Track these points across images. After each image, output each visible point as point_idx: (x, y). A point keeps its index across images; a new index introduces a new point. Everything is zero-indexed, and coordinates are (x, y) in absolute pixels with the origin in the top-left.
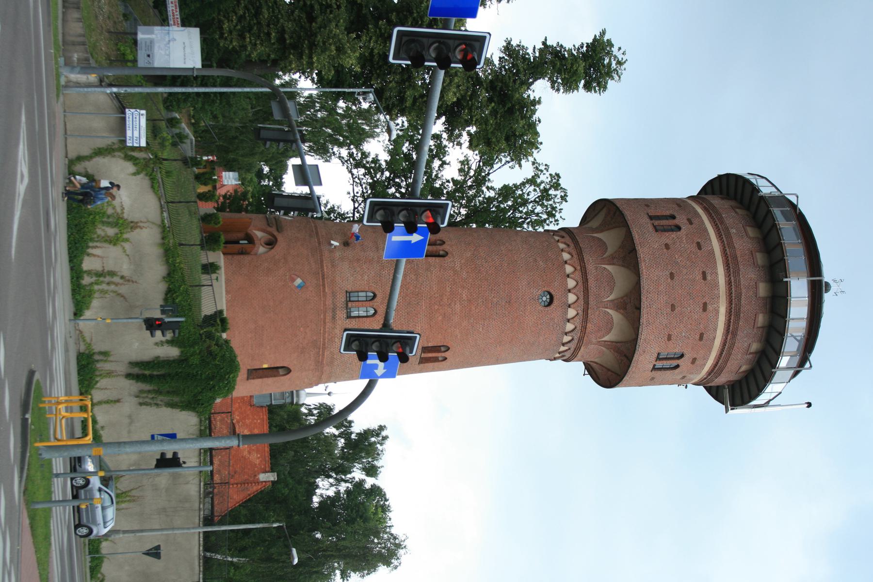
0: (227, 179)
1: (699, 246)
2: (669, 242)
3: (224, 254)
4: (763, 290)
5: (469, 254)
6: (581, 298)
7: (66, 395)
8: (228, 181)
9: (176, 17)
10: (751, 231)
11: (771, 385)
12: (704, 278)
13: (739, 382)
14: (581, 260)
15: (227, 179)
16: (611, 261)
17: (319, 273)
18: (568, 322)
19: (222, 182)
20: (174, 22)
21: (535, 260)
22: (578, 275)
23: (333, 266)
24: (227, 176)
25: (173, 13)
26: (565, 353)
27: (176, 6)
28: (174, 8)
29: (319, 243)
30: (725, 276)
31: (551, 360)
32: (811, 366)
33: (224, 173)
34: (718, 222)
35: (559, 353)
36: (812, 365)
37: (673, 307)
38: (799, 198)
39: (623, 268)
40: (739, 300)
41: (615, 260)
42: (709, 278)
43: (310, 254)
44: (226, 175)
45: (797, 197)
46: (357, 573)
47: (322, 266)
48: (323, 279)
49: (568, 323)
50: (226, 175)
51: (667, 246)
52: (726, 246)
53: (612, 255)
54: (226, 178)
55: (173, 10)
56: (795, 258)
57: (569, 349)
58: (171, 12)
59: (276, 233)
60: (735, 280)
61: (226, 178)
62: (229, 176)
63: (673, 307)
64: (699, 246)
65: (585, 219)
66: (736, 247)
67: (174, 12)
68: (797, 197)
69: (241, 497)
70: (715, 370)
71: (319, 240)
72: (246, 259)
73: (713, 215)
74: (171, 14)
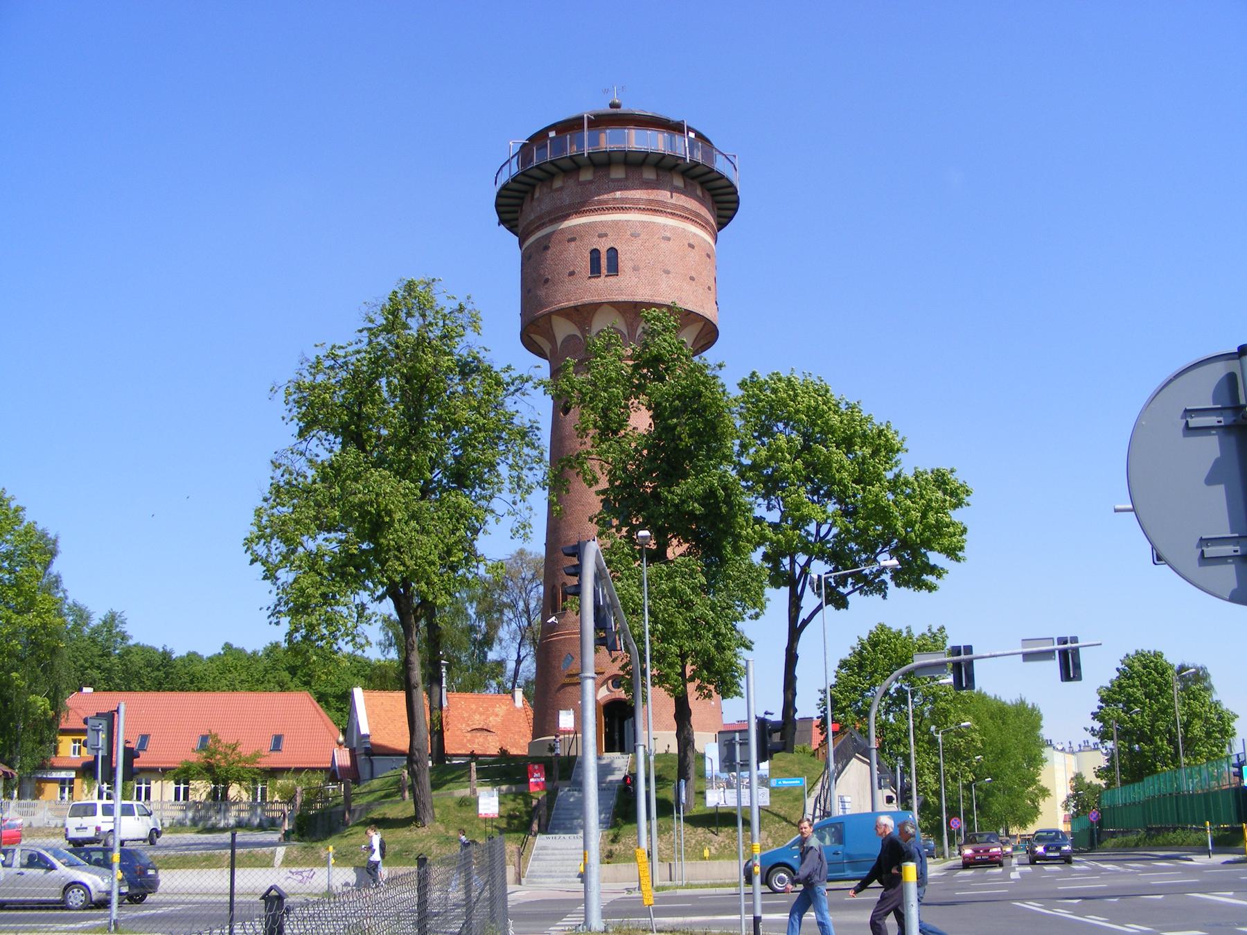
2: (630, 264)
7: (94, 814)
10: (558, 184)
12: (669, 239)
24: (486, 807)
30: (667, 217)
34: (604, 207)
38: (630, 106)
40: (687, 209)
42: (668, 234)
46: (547, 727)
51: (636, 269)
54: (489, 809)
56: (609, 140)
60: (671, 208)
61: (489, 809)
62: (485, 804)
65: (541, 354)
69: (508, 851)
73: (624, 206)
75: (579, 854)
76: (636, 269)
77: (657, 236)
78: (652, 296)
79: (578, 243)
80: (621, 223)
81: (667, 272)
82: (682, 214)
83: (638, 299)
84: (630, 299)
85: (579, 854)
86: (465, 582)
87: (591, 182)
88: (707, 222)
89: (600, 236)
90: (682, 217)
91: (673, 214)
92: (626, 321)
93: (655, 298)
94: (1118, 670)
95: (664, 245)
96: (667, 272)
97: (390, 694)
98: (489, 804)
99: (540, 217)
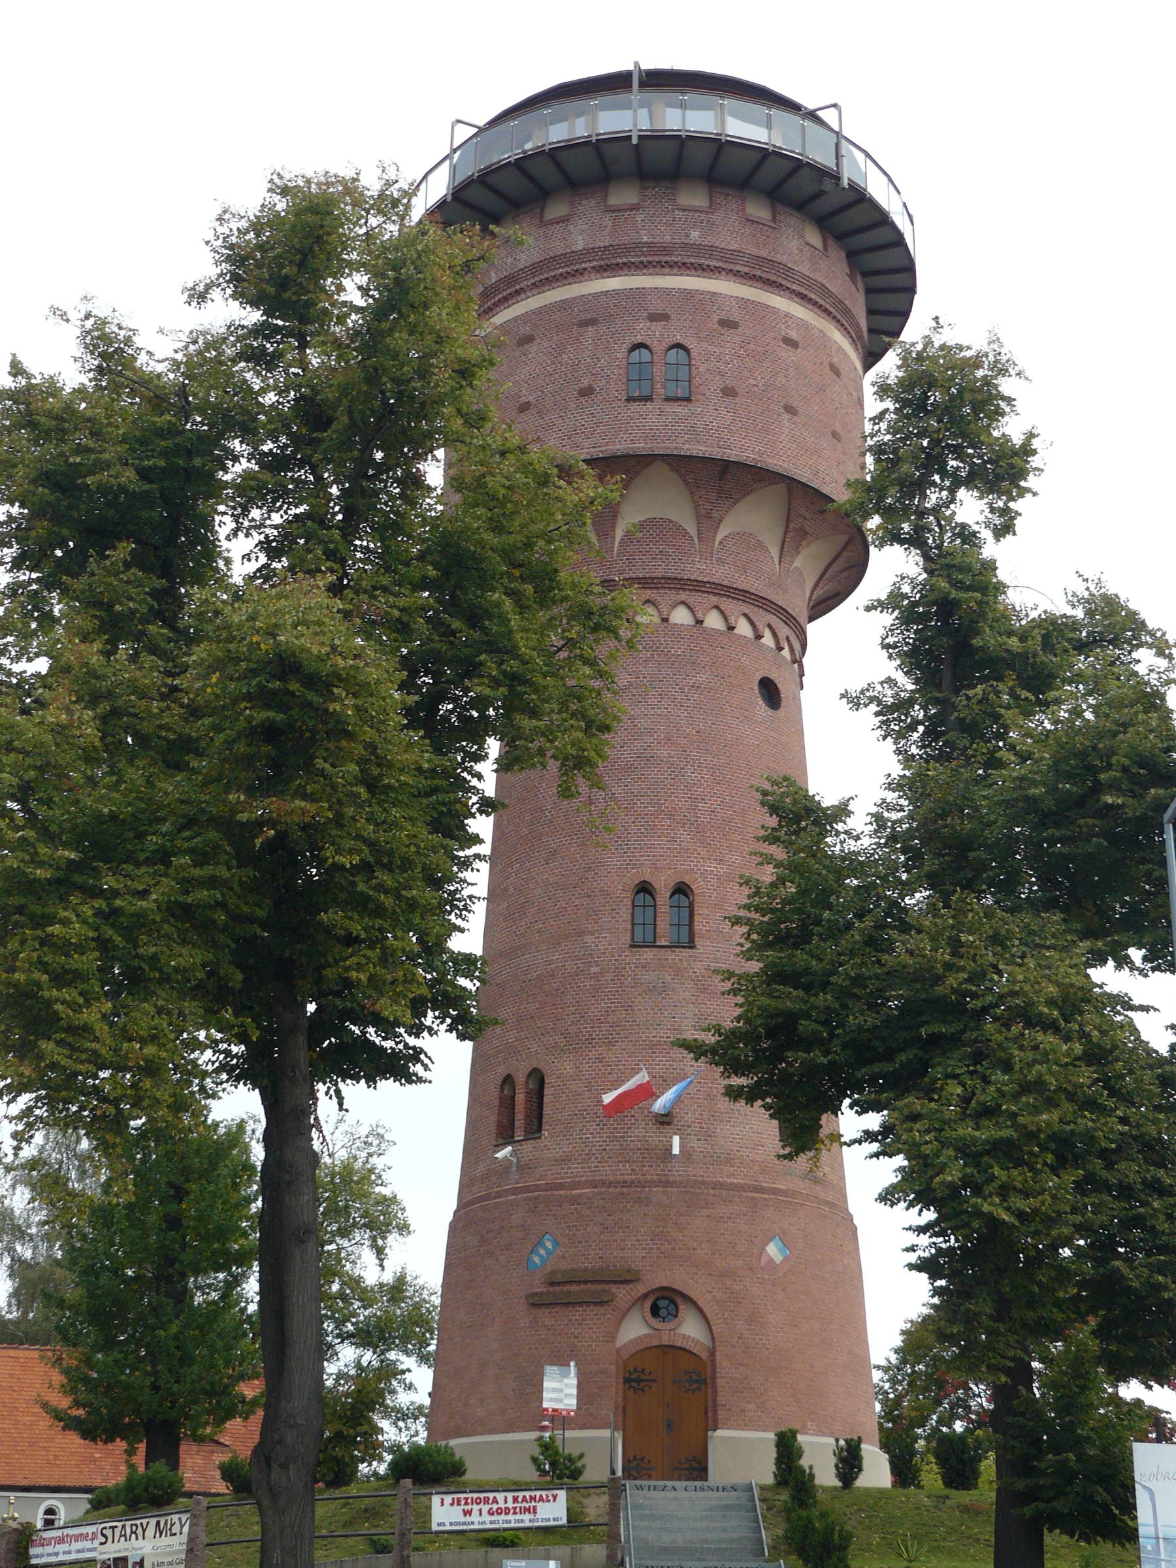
0: (561, 1396)
1: (728, 324)
2: (717, 383)
3: (715, 1430)
4: (693, 197)
5: (683, 835)
6: (683, 596)
8: (567, 1395)
9: (510, 1504)
11: (869, 190)
13: (852, 256)
14: (697, 586)
15: (561, 1396)
16: (708, 521)
17: (752, 1199)
18: (702, 622)
19: (568, 1412)
20: (527, 1510)
21: (696, 687)
22: (665, 598)
23: (728, 1162)
24: (554, 1396)
25: (499, 1512)
26: (782, 636)
27: (478, 1502)
28: (485, 1508)
29: (667, 1184)
31: (802, 674)
32: (835, 106)
33: (545, 1405)
35: (780, 649)
36: (833, 102)
37: (587, 392)
39: (749, 498)
41: (715, 514)
42: (793, 335)
43: (704, 1212)
44: (552, 1400)
45: (459, 121)
47: (733, 1187)
48: (763, 1190)
49: (705, 624)
50: (552, 1400)
52: (731, 267)
53: (698, 517)
54: (561, 1401)
55: (491, 1513)
57: (769, 626)
58: (495, 1517)
59: (641, 1289)
60: (801, 284)
61: (561, 1401)
62: (554, 1390)
63: (587, 392)
64: (728, 324)
66: (734, 246)
67: (495, 1506)
68: (459, 121)
70: (835, 312)
71: (653, 1184)
72: (726, 1372)
74: (503, 1517)
75: (37, 1556)
76: (729, 392)
77: (771, 335)
78: (761, 454)
79: (603, 329)
80: (697, 297)
81: (791, 410)
82: (821, 302)
83: (733, 455)
84: (717, 453)
85: (37, 1556)
86: (459, 900)
87: (634, 208)
88: (860, 337)
89: (653, 318)
90: (826, 310)
91: (803, 297)
92: (696, 507)
93: (769, 460)
94: (922, 1266)
95: (786, 353)
96: (791, 410)
97: (12, 1353)
98: (561, 1391)
99: (509, 280)
